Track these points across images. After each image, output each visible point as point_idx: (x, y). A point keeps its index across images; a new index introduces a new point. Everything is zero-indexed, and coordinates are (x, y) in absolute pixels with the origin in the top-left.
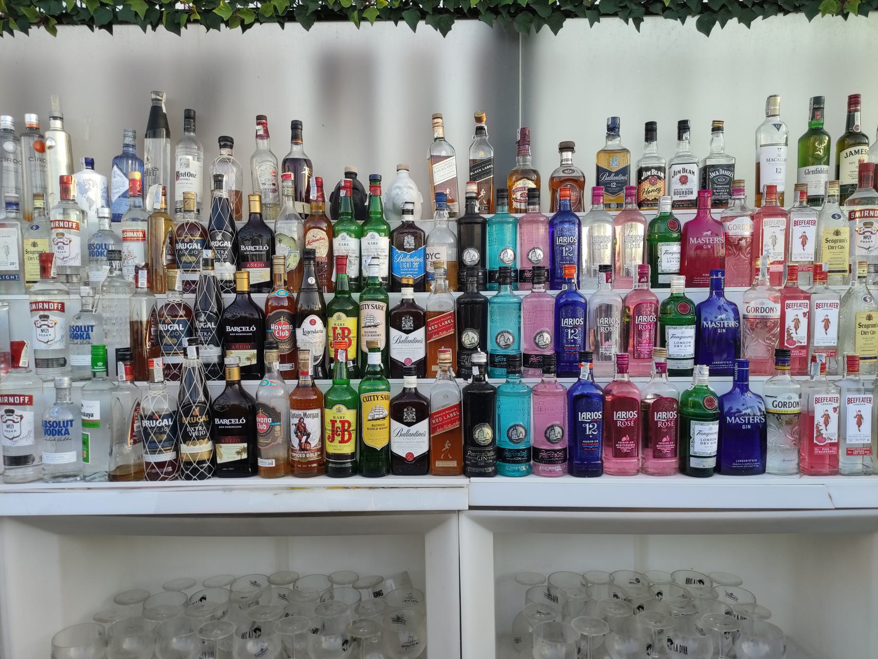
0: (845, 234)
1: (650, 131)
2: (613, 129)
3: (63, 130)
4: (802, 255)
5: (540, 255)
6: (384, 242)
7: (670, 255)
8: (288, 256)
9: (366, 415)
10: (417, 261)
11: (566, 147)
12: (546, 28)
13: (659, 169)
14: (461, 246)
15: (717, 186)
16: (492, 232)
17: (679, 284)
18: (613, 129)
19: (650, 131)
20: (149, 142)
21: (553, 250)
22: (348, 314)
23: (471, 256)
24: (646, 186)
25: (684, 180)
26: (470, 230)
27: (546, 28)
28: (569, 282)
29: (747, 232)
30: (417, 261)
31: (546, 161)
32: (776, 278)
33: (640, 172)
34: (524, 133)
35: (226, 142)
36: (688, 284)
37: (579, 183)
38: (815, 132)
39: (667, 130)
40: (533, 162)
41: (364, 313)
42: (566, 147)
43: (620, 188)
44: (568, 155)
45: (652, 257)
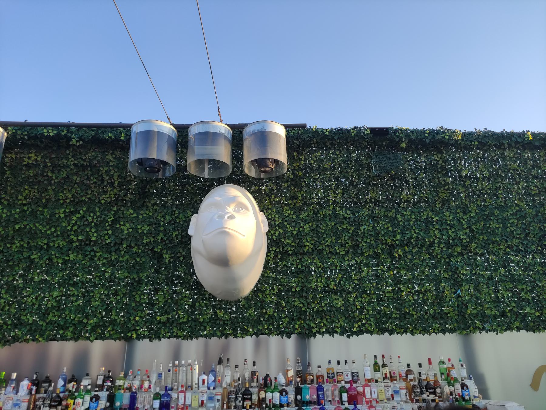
0: (383, 391)
1: (339, 363)
2: (330, 362)
3: (67, 400)
4: (375, 396)
5: (315, 397)
6: (278, 394)
7: (345, 396)
8: (255, 397)
9: (85, 400)
10: (286, 399)
11: (319, 367)
12: (312, 337)
13: (342, 373)
14: (296, 395)
15: (355, 378)
16: (303, 390)
17: (346, 404)
18: (330, 362)
19: (339, 363)
20: (218, 366)
21: (318, 396)
22: (81, 398)
23: (299, 397)
24: (339, 377)
25: (347, 376)
26: (298, 391)
27: (312, 337)
28: (322, 404)
29: (362, 390)
30: (286, 399)
31: (314, 370)
32: (367, 402)
33: (337, 373)
34: (309, 363)
35: (237, 366)
36: (349, 404)
37: (323, 376)
38: (376, 364)
39: (342, 362)
40: (312, 370)
41: (85, 398)
42: (319, 367)
43: (332, 377)
44: (320, 369)
45: (341, 398)
